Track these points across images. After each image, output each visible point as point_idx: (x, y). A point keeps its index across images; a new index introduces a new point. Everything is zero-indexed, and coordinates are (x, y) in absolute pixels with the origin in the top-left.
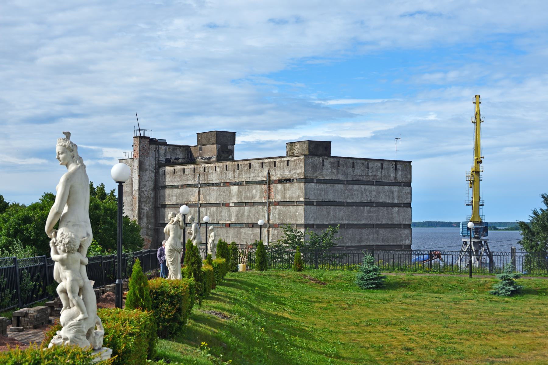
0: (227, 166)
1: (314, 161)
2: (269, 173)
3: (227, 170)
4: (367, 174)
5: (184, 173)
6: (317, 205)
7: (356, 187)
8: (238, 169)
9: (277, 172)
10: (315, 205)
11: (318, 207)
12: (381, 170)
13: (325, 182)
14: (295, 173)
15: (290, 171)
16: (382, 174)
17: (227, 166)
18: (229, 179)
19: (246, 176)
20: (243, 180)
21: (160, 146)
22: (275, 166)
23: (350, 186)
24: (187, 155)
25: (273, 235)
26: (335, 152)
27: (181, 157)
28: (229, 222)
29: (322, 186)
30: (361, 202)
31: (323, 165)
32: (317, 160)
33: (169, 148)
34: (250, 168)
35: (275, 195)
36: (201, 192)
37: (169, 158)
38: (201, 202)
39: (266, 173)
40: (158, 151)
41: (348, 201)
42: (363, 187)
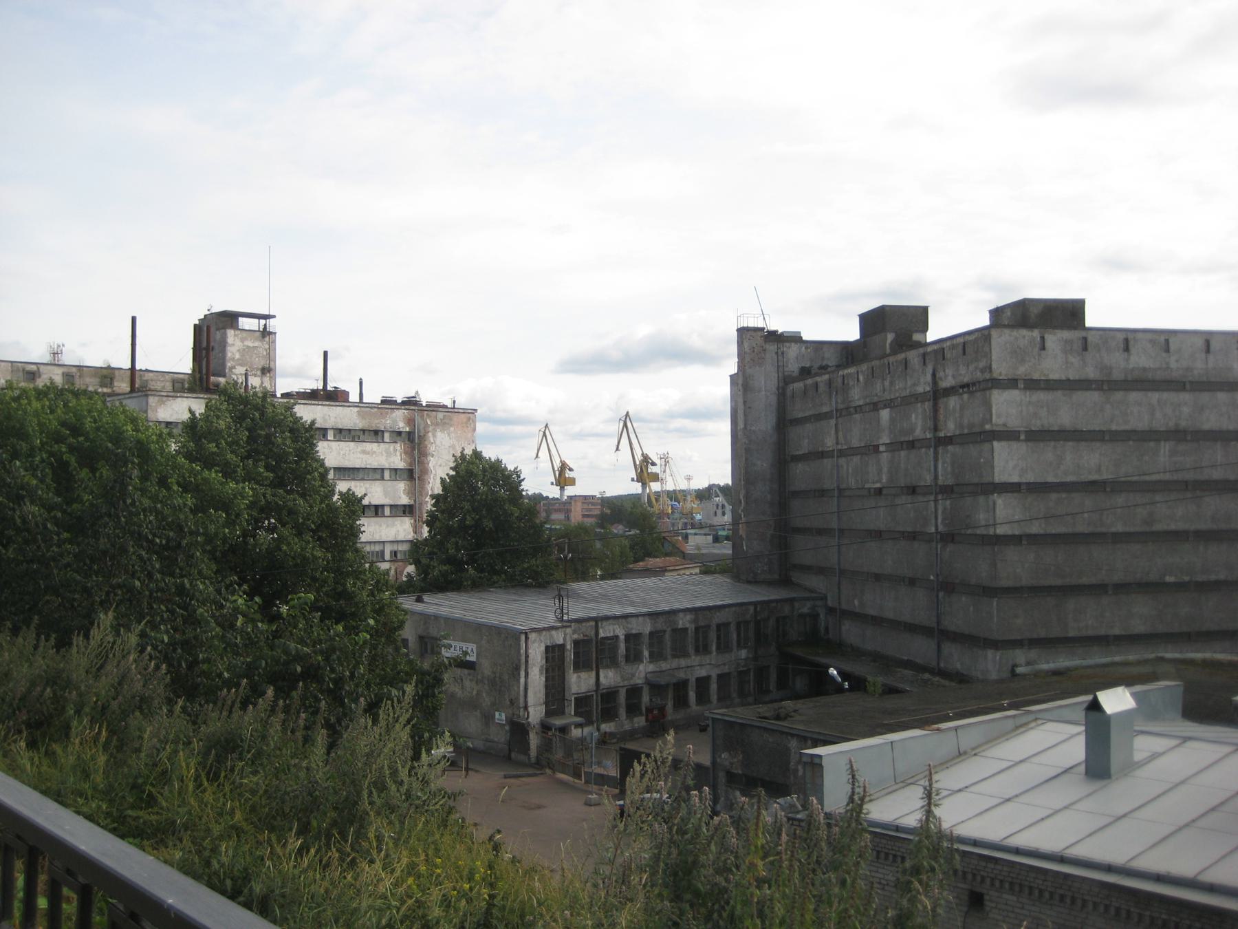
0: (873, 368)
1: (1016, 339)
2: (934, 375)
3: (873, 377)
4: (1164, 366)
5: (817, 391)
6: (1027, 440)
7: (1134, 396)
8: (889, 373)
9: (947, 371)
10: (1022, 441)
11: (1030, 444)
12: (1203, 355)
13: (1050, 385)
14: (976, 368)
15: (968, 366)
16: (1207, 364)
17: (873, 368)
18: (877, 395)
19: (901, 385)
20: (897, 395)
21: (787, 344)
22: (944, 359)
23: (1119, 395)
24: (844, 360)
25: (945, 509)
26: (1093, 319)
27: (834, 363)
28: (878, 485)
29: (1042, 396)
30: (1150, 431)
31: (1043, 348)
32: (1024, 337)
33: (806, 348)
34: (906, 368)
35: (945, 421)
36: (840, 427)
37: (807, 366)
38: (839, 447)
39: (929, 378)
40: (783, 353)
41: (1114, 427)
42: (1154, 397)
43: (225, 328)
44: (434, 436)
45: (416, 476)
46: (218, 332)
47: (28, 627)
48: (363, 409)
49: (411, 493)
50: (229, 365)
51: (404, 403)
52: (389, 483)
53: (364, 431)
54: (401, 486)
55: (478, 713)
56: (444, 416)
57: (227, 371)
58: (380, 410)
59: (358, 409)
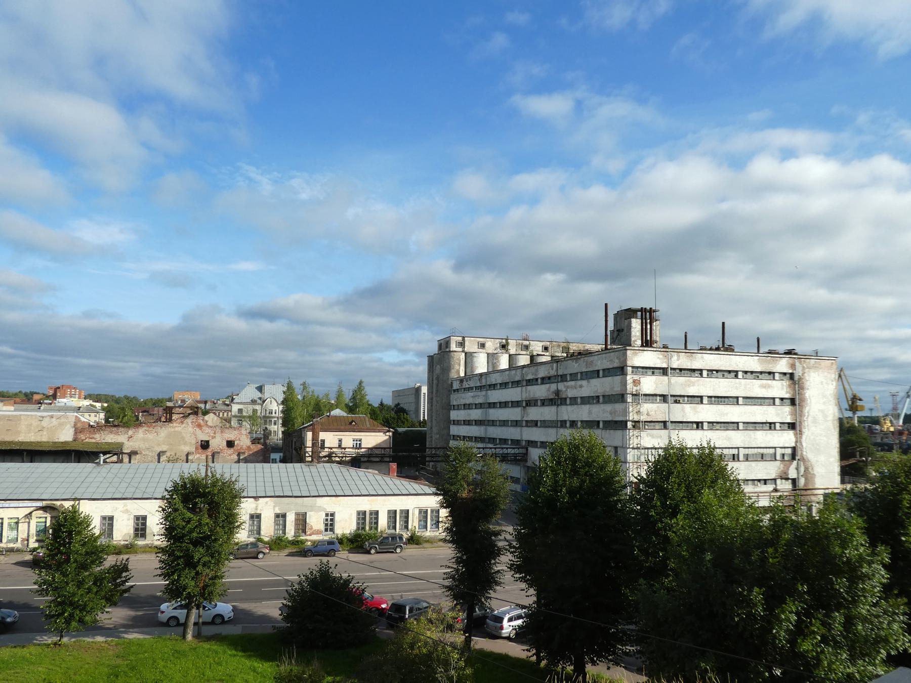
43: (630, 318)
44: (809, 376)
45: (797, 403)
46: (626, 321)
47: (820, 624)
48: (761, 357)
49: (794, 414)
50: (633, 339)
51: (785, 353)
52: (779, 407)
53: (761, 373)
54: (787, 409)
55: (529, 464)
56: (815, 362)
57: (632, 343)
58: (773, 358)
59: (758, 357)
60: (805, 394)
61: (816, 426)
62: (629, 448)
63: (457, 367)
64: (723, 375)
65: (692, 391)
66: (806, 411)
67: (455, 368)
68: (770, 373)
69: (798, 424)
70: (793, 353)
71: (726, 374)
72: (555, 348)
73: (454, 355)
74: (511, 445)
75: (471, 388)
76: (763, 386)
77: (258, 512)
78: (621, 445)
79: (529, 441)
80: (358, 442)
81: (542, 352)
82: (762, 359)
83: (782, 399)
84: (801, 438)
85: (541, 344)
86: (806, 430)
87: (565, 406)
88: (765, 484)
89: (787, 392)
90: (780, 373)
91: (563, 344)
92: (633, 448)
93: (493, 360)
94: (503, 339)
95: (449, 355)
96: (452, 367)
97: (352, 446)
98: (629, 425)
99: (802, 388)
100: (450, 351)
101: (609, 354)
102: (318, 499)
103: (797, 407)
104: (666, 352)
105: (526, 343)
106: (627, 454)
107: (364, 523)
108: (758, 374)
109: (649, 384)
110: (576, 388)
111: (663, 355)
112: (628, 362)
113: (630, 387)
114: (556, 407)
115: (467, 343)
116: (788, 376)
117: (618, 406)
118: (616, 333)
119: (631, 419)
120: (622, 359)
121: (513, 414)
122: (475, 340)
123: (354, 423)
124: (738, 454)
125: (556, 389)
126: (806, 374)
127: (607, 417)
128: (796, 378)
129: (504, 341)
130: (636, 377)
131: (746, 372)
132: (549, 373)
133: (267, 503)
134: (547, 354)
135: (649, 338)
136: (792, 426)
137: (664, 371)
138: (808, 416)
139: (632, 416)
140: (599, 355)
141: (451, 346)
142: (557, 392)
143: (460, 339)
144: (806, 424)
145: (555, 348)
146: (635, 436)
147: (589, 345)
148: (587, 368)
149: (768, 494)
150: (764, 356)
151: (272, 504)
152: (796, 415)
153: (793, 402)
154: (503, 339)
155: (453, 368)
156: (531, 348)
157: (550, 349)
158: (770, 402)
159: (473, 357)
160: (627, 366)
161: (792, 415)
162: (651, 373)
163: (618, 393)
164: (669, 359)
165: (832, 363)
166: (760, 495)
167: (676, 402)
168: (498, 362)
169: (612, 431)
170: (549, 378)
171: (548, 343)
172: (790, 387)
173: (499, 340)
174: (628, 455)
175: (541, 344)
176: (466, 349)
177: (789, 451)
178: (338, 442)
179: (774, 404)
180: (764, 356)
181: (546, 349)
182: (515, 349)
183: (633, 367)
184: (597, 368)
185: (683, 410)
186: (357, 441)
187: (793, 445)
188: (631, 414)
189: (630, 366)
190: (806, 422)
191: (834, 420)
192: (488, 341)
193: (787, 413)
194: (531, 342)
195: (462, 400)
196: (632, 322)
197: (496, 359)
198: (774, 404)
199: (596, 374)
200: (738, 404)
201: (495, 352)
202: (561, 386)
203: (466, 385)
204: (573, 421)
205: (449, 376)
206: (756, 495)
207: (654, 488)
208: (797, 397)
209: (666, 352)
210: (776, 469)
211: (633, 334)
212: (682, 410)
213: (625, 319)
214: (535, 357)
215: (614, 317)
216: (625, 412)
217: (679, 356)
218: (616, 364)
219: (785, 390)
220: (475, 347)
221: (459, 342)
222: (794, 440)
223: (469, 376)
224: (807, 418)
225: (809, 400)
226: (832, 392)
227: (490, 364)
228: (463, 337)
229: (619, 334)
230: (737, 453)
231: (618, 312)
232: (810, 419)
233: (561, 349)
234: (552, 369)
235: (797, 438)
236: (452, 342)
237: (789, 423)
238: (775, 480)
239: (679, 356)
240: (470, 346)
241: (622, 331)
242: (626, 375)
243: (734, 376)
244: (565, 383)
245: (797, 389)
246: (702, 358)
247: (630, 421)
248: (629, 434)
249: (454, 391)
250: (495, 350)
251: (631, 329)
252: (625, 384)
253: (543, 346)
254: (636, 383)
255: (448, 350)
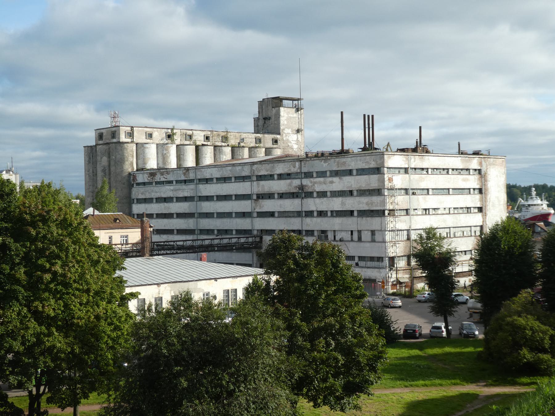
45: (483, 192)
46: (273, 109)
49: (482, 200)
50: (282, 128)
53: (462, 169)
54: (478, 196)
56: (494, 160)
59: (461, 158)
60: (488, 185)
61: (494, 209)
62: (387, 231)
63: (130, 159)
64: (440, 172)
65: (423, 185)
66: (488, 198)
67: (129, 160)
68: (467, 170)
69: (484, 208)
70: (480, 153)
71: (442, 171)
72: (216, 138)
73: (128, 146)
74: (236, 234)
75: (170, 182)
76: (464, 180)
77: (160, 296)
78: (379, 228)
79: (262, 230)
80: (125, 239)
81: (204, 141)
82: (464, 159)
83: (474, 189)
84: (486, 218)
85: (202, 134)
86: (489, 212)
87: (312, 199)
88: (465, 254)
89: (478, 184)
90: (473, 169)
91: (223, 134)
92: (389, 231)
93: (163, 150)
94: (169, 129)
95: (122, 147)
96: (126, 159)
97: (120, 243)
98: (387, 212)
99: (486, 181)
100: (119, 143)
101: (365, 157)
102: (199, 283)
103: (484, 194)
104: (407, 155)
105: (190, 132)
106: (386, 235)
107: (228, 300)
108: (460, 171)
109: (399, 181)
110: (325, 184)
111: (405, 158)
112: (385, 164)
113: (387, 184)
114: (301, 199)
115: (135, 134)
116: (477, 171)
117: (376, 199)
118: (261, 122)
119: (388, 208)
120: (379, 162)
121: (245, 206)
122: (143, 130)
123: (118, 221)
124: (450, 233)
125: (300, 184)
126: (488, 170)
127: (364, 207)
128: (483, 173)
129: (169, 131)
130: (390, 176)
131: (453, 169)
132: (290, 170)
133: (165, 288)
134: (209, 143)
135: (371, 141)
136: (480, 209)
137: (406, 170)
138: (490, 201)
139: (389, 206)
140: (352, 157)
141: (121, 136)
142: (302, 187)
143: (129, 129)
144: (489, 208)
145: (216, 138)
146: (390, 221)
147: (245, 134)
148: (338, 167)
149: (467, 262)
150: (464, 157)
151: (169, 289)
152: (483, 201)
153: (480, 191)
154: (169, 129)
155: (127, 161)
156: (194, 138)
157: (211, 139)
158: (467, 192)
159: (145, 148)
160: (384, 167)
161: (480, 201)
162: (397, 172)
163: (375, 188)
164: (409, 161)
165: (503, 161)
166: (464, 262)
167: (414, 194)
168: (168, 153)
169: (369, 219)
170: (289, 175)
171: (209, 133)
172: (479, 180)
173: (165, 130)
174: (386, 236)
175: (202, 134)
176: (135, 140)
177: (478, 228)
178: (108, 239)
179: (470, 193)
180: (464, 157)
181: (207, 138)
182: (179, 139)
183: (388, 168)
184: (350, 168)
185: (418, 200)
186: (123, 237)
187: (481, 224)
188: (388, 204)
189: (386, 167)
190: (488, 206)
191: (504, 204)
192: (155, 131)
193: (478, 200)
194: (194, 132)
195: (140, 195)
196: (281, 111)
197: (166, 150)
198: (470, 193)
199: (350, 173)
200: (449, 194)
201: (162, 142)
202: (306, 182)
203: (158, 178)
204: (320, 211)
205: (123, 168)
206: (461, 263)
207: (274, 278)
208: (483, 187)
209: (407, 155)
210: (472, 243)
211: (282, 122)
212: (418, 200)
213: (273, 107)
214: (200, 147)
215: (259, 104)
216: (384, 203)
217: (415, 158)
218: (373, 165)
219: (476, 182)
220: (143, 137)
221: (128, 133)
222: (482, 220)
223: (162, 170)
224: (489, 203)
225: (490, 189)
226: (503, 183)
227: (160, 155)
228: (132, 127)
229: (265, 122)
230: (449, 232)
231: (263, 99)
232: (491, 204)
233: (221, 138)
234: (295, 167)
235: (483, 219)
236: (121, 132)
237: (478, 208)
238: (471, 251)
239: (415, 158)
240: (140, 137)
241: (269, 119)
242: (384, 174)
243: (446, 173)
244: (312, 179)
245: (483, 181)
246: (429, 159)
247: (387, 210)
248: (387, 220)
249: (138, 184)
250: (162, 140)
251: (279, 117)
252: (383, 181)
253: (204, 136)
254: (390, 180)
255: (115, 140)
